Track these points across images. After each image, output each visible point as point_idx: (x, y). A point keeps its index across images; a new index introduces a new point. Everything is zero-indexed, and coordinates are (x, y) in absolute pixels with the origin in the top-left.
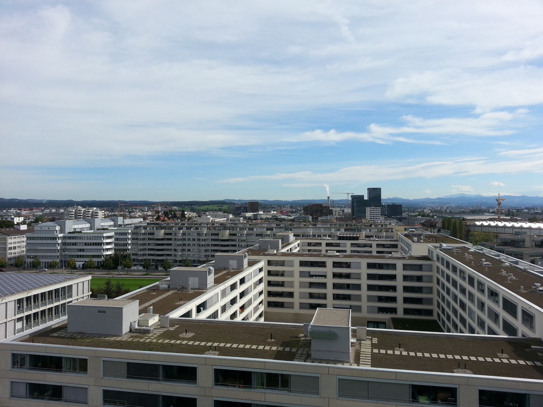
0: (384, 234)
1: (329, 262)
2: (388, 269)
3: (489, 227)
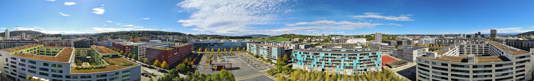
1: (471, 46)
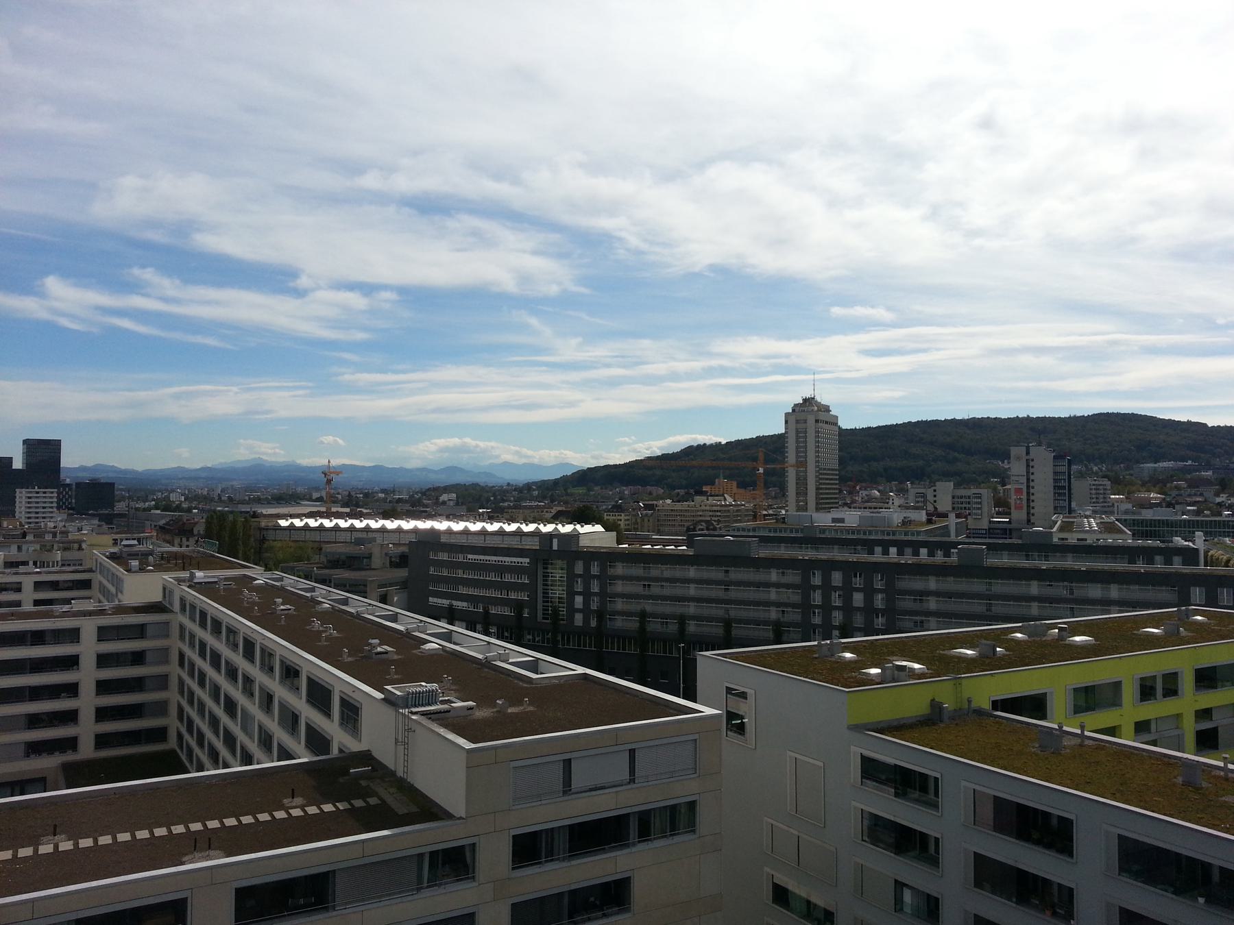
0: (58, 556)
2: (58, 643)
3: (305, 530)
